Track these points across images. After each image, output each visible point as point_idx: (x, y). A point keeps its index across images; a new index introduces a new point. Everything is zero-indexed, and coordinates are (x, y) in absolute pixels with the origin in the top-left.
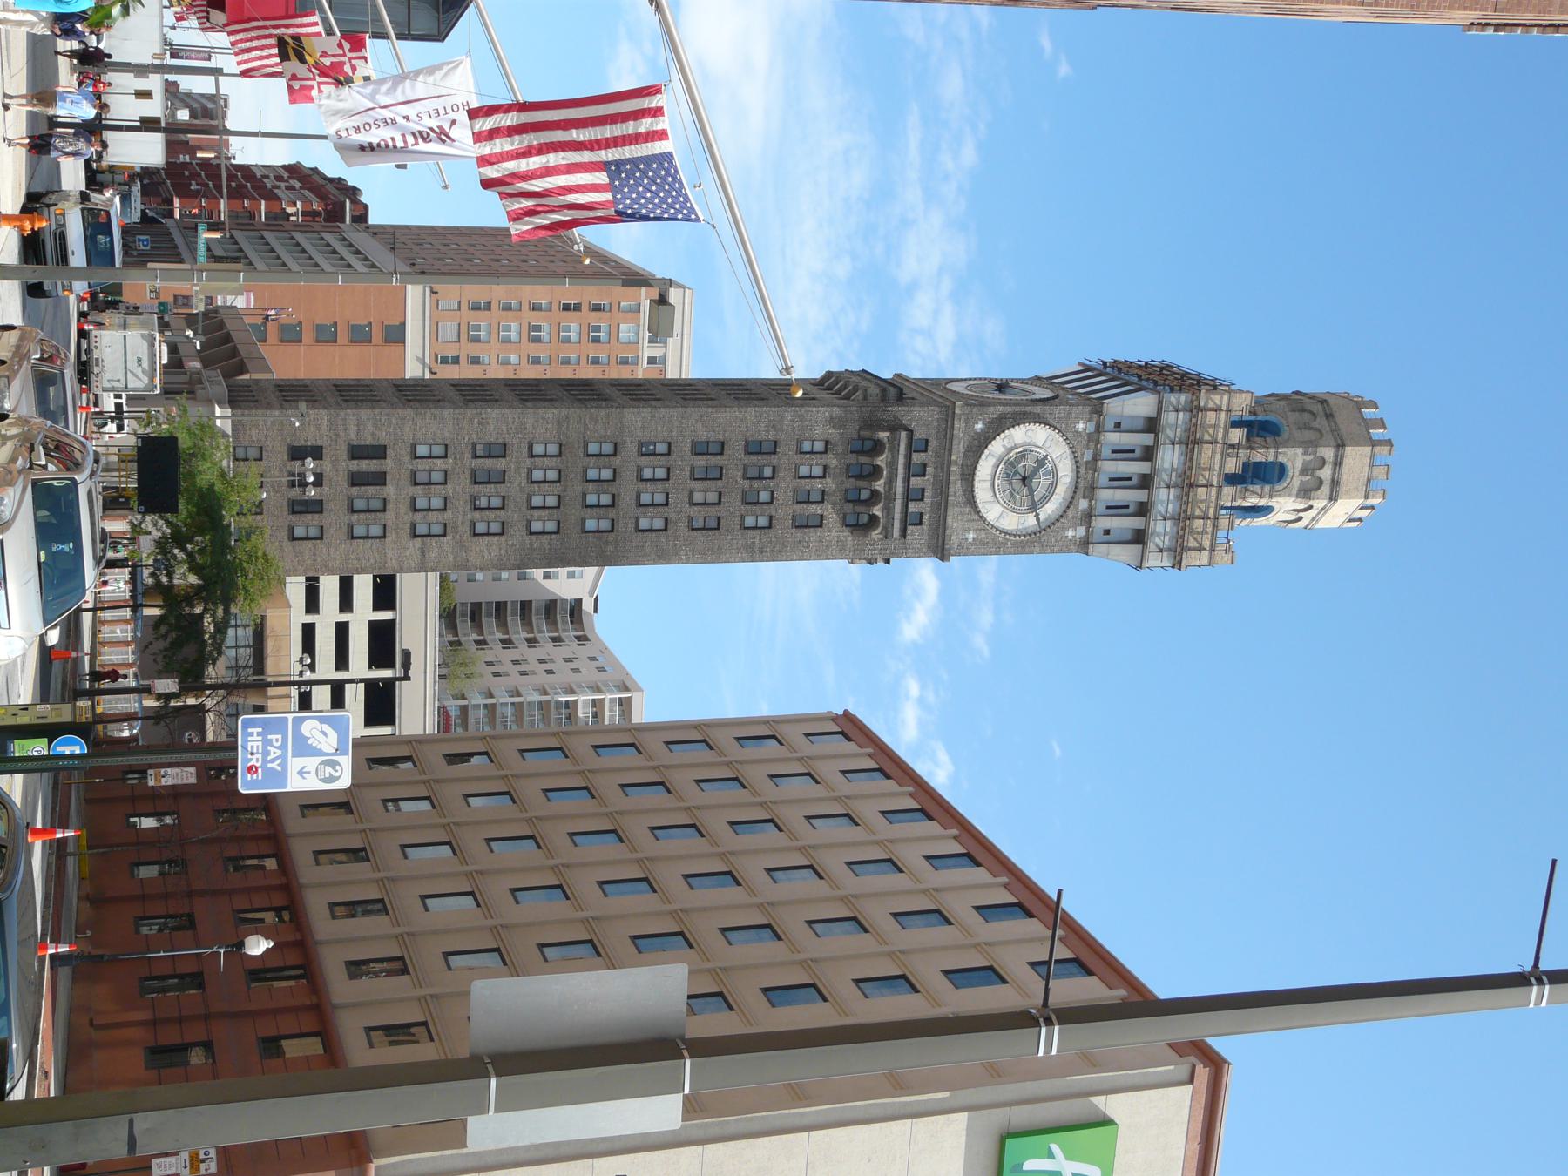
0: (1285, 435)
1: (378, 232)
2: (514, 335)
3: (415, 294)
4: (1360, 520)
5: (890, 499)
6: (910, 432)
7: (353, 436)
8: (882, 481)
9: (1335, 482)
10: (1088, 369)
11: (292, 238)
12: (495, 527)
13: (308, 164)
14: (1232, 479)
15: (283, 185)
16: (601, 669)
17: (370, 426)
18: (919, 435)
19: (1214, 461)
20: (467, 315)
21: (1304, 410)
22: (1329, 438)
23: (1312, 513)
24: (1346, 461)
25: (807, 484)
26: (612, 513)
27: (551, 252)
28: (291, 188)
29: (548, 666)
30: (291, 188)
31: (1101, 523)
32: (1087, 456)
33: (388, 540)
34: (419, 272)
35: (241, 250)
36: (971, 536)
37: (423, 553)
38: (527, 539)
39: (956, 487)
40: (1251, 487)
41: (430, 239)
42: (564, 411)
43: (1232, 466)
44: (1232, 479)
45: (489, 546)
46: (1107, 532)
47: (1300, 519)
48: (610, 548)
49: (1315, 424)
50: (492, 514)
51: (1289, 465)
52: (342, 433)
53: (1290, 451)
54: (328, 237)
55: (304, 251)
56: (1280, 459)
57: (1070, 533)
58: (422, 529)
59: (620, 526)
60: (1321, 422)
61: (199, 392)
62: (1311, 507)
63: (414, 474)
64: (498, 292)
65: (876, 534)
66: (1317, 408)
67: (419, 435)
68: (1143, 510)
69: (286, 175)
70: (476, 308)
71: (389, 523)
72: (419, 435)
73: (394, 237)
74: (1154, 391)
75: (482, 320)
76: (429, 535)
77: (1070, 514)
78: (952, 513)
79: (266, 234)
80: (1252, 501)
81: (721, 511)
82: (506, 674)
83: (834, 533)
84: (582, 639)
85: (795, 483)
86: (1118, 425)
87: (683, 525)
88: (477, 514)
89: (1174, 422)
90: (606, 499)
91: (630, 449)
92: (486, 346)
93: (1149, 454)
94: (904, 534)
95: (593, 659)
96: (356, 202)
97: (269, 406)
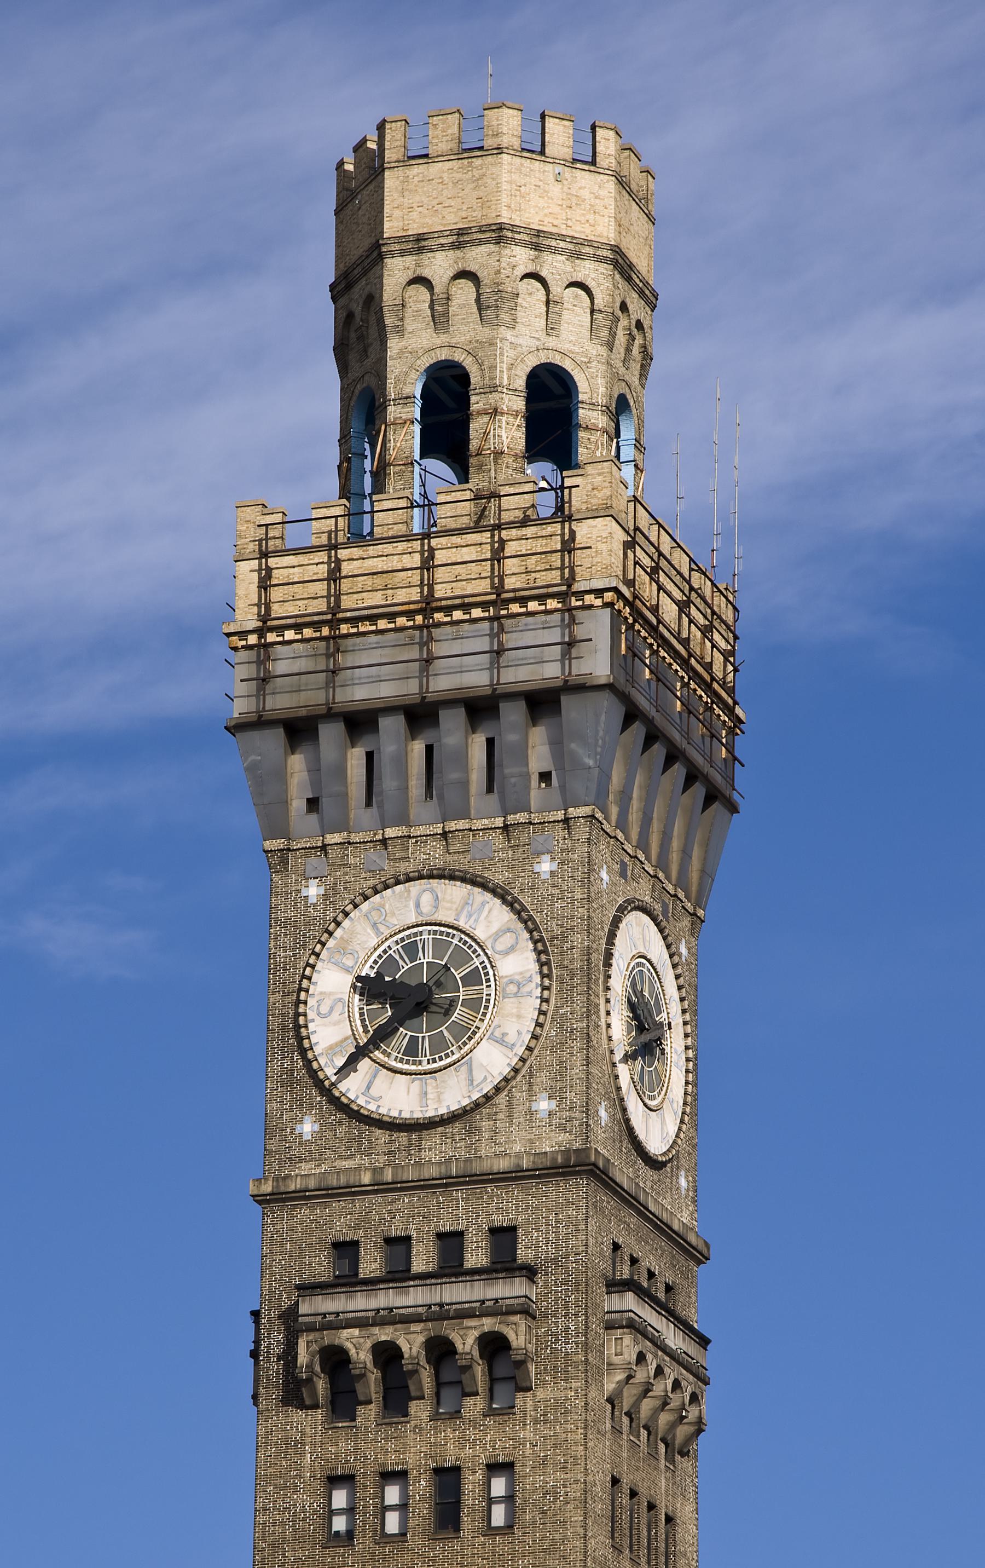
5: (441, 1313)
36: (544, 1105)
39: (435, 1152)
65: (518, 1335)
77: (498, 877)
83: (527, 1434)
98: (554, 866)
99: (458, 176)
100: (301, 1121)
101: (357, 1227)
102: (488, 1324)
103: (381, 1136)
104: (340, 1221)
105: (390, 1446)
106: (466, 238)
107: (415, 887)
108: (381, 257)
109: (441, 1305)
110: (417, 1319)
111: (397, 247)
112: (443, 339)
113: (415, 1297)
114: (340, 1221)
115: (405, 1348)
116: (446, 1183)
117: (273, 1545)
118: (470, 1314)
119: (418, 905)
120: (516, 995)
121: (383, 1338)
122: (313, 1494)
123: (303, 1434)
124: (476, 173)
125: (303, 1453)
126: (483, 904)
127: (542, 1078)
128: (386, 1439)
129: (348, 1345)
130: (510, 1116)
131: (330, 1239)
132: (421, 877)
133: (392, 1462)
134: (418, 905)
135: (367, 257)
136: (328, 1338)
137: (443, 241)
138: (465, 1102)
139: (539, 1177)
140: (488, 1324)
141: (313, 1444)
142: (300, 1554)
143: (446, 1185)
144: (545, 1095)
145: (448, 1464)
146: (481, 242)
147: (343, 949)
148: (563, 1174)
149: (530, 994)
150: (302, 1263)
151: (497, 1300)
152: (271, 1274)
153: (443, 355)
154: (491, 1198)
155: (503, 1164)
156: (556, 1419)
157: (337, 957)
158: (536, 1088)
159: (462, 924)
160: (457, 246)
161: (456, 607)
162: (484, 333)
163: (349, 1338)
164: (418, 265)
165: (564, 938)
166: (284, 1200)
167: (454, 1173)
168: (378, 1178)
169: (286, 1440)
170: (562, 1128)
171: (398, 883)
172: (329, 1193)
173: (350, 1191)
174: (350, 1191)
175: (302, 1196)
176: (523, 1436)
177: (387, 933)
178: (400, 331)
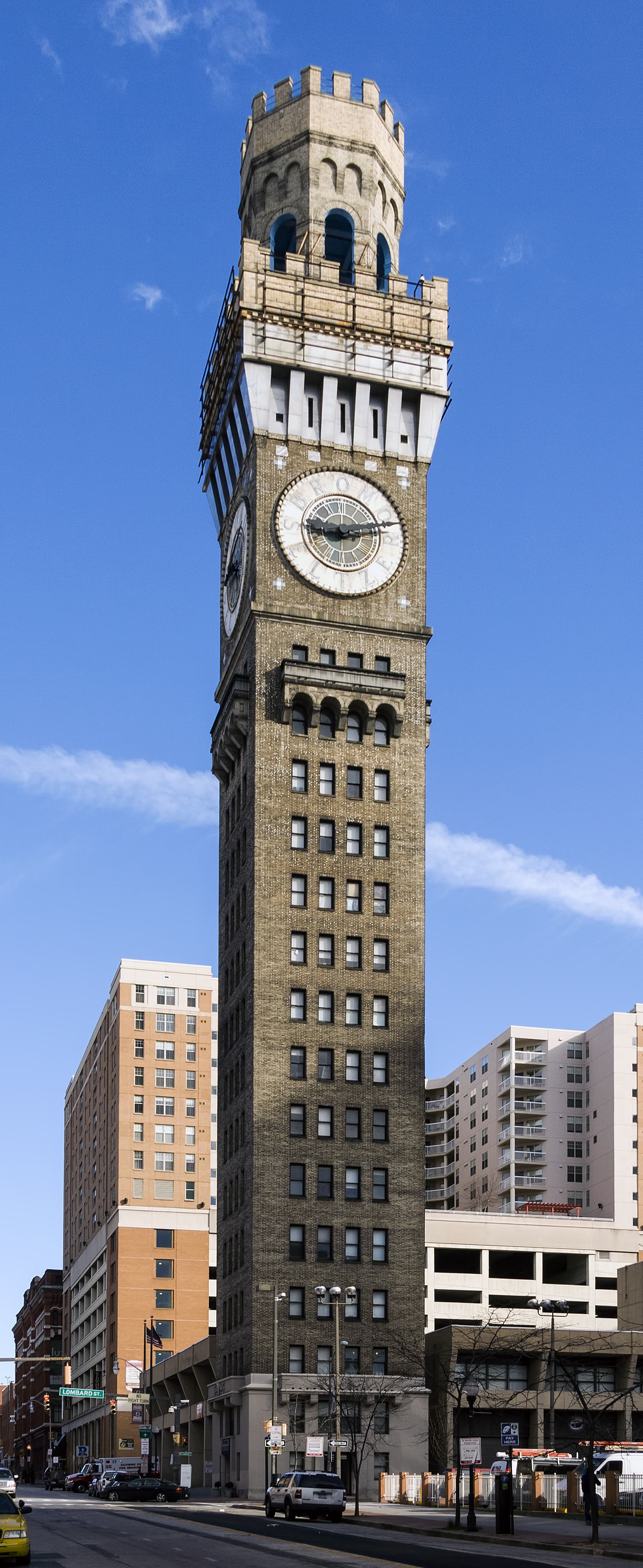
0: (294, 211)
1: (70, 1259)
2: (169, 1130)
3: (127, 1218)
4: (396, 126)
5: (360, 689)
6: (285, 662)
7: (280, 1256)
8: (340, 699)
9: (353, 145)
10: (211, 476)
11: (77, 1330)
12: (379, 1119)
13: (14, 1321)
14: (347, 278)
15: (31, 1341)
16: (485, 1069)
17: (268, 1240)
18: (288, 653)
19: (326, 299)
20: (148, 1171)
21: (263, 192)
22: (296, 156)
23: (387, 184)
24: (328, 131)
25: (341, 785)
26: (368, 997)
27: (86, 1104)
28: (33, 1335)
29: (479, 1118)
30: (33, 1335)
31: (395, 447)
32: (314, 456)
33: (390, 1227)
34: (110, 1205)
35: (88, 1373)
36: (404, 602)
37: (404, 1192)
38: (392, 1087)
39: (348, 612)
40: (356, 258)
41: (75, 1236)
42: (256, 1042)
43: (331, 272)
44: (347, 278)
45: (399, 1125)
46: (404, 439)
47: (392, 201)
48: (405, 1001)
49: (281, 173)
50: (366, 1121)
51: (331, 206)
52: (277, 1267)
53: (313, 205)
54: (74, 1302)
55: (88, 1346)
56: (323, 218)
57: (404, 484)
58: (379, 1194)
59: (381, 989)
60: (279, 167)
61: (233, 1401)
62: (380, 184)
63: (320, 1198)
64: (126, 1145)
65: (400, 709)
66: (261, 174)
67: (281, 1191)
68: (379, 392)
69: (23, 1339)
70: (140, 1164)
71: (371, 1224)
72: (281, 1191)
73: (75, 1242)
74: (241, 371)
75: (153, 1159)
76: (386, 1186)
77: (381, 482)
78: (375, 619)
79: (73, 1328)
80: (370, 258)
81: (368, 879)
82: (485, 1155)
83: (396, 758)
84: (451, 1089)
85: (339, 798)
86: (279, 417)
87: (384, 922)
88: (366, 1136)
89: (279, 344)
90: (350, 1004)
91: (301, 975)
92: (177, 1157)
93: (314, 381)
94: (401, 677)
95: (473, 1077)
96: (43, 1281)
97: (248, 1337)
98: (409, 485)
99: (350, 112)
100: (276, 580)
101: (307, 640)
102: (385, 700)
103: (319, 598)
104: (299, 634)
105: (326, 751)
106: (355, 146)
107: (337, 475)
108: (308, 140)
109: (361, 685)
110: (349, 690)
111: (318, 138)
112: (338, 197)
113: (347, 679)
114: (299, 634)
115: (342, 702)
116: (355, 628)
117: (265, 786)
118: (377, 693)
119: (338, 485)
120: (390, 543)
121: (330, 695)
122: (286, 766)
123: (280, 736)
124: (360, 115)
125: (280, 745)
126: (373, 493)
127: (403, 588)
128: (324, 746)
129: (311, 695)
130: (386, 603)
131: (292, 643)
132: (340, 470)
133: (327, 759)
134: (338, 485)
135: (294, 141)
136: (301, 689)
137: (343, 143)
138: (364, 591)
139: (402, 636)
140: (385, 700)
141: (286, 742)
142: (279, 793)
143: (354, 629)
144: (405, 597)
145: (356, 765)
146: (363, 152)
147: (297, 497)
148: (415, 638)
149: (397, 545)
150: (277, 651)
151: (389, 689)
152: (261, 653)
153: (340, 206)
154: (377, 641)
155: (386, 625)
156: (411, 755)
157: (294, 500)
158: (400, 593)
159: (361, 500)
160: (350, 149)
161: (368, 332)
162: (362, 201)
163: (311, 691)
164: (328, 152)
165: (414, 523)
166: (268, 617)
167: (361, 623)
168: (321, 617)
169: (271, 737)
170: (413, 615)
171: (328, 470)
172: (294, 619)
173: (304, 620)
174: (304, 620)
175: (279, 617)
176: (394, 759)
177: (322, 495)
178: (317, 185)
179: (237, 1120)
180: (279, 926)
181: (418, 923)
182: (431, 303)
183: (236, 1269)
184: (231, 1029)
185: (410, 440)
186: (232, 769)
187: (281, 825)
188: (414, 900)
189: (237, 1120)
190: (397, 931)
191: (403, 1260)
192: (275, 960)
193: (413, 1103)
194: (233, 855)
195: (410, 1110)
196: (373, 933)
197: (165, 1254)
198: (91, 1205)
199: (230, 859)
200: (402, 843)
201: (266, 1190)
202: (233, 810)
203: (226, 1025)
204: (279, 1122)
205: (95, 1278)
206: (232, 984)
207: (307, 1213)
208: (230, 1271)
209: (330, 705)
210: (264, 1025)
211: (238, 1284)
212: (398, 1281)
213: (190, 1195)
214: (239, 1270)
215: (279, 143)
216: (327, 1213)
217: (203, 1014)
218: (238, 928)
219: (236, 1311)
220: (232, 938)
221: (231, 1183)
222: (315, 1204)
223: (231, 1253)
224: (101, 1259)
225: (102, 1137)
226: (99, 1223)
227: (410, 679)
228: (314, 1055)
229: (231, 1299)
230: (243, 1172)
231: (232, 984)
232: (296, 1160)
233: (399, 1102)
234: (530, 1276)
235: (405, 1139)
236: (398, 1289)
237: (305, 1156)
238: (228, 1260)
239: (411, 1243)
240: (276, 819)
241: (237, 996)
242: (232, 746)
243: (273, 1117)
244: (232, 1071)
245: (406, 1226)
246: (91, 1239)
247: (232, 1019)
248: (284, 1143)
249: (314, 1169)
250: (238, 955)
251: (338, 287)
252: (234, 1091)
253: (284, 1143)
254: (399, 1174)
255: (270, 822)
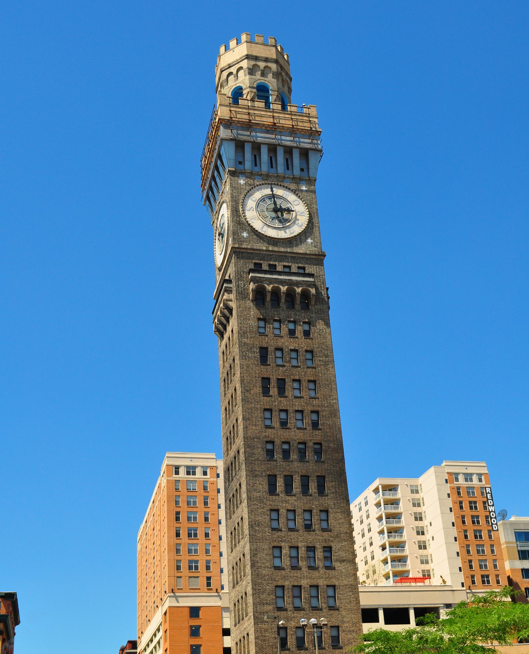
33: (337, 584)
37: (343, 561)
48: (332, 445)
49: (235, 72)
67: (268, 564)
71: (325, 583)
168: (268, 249)
169: (245, 307)
179: (238, 524)
180: (256, 406)
181: (334, 401)
182: (309, 114)
183: (243, 619)
184: (232, 470)
185: (305, 170)
186: (225, 329)
187: (254, 352)
188: (331, 388)
189: (238, 524)
190: (323, 406)
191: (346, 605)
192: (256, 425)
193: (342, 505)
194: (228, 374)
195: (341, 509)
196: (310, 408)
197: (195, 622)
198: (152, 597)
199: (226, 376)
200: (321, 359)
201: (259, 565)
202: (226, 351)
203: (229, 469)
204: (264, 521)
205: (155, 641)
206: (231, 444)
207: (284, 578)
208: (239, 621)
209: (276, 293)
210: (252, 463)
211: (245, 629)
212: (345, 620)
213: (209, 584)
214: (246, 619)
215: (233, 61)
216: (297, 577)
217: (212, 479)
218: (233, 411)
219: (244, 647)
220: (229, 418)
221: (237, 564)
222: (290, 572)
223: (238, 609)
224: (158, 630)
225: (158, 540)
226: (157, 606)
227: (317, 276)
228: (282, 479)
229: (240, 640)
230: (244, 555)
231: (231, 444)
232: (276, 544)
233: (334, 505)
234: (377, 621)
235: (340, 527)
236: (345, 625)
237: (281, 541)
238: (237, 614)
239: (351, 593)
240: (251, 349)
241: (234, 450)
242: (221, 323)
243: (260, 518)
244: (233, 496)
245: (347, 583)
246: (152, 617)
247: (232, 464)
248: (268, 534)
249: (288, 549)
250: (233, 427)
251: (264, 109)
252: (235, 506)
253: (268, 534)
254: (339, 550)
255: (248, 351)
